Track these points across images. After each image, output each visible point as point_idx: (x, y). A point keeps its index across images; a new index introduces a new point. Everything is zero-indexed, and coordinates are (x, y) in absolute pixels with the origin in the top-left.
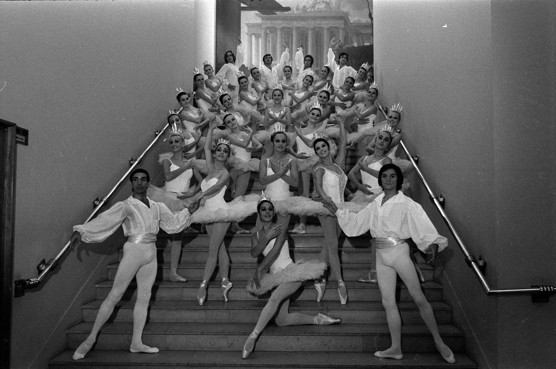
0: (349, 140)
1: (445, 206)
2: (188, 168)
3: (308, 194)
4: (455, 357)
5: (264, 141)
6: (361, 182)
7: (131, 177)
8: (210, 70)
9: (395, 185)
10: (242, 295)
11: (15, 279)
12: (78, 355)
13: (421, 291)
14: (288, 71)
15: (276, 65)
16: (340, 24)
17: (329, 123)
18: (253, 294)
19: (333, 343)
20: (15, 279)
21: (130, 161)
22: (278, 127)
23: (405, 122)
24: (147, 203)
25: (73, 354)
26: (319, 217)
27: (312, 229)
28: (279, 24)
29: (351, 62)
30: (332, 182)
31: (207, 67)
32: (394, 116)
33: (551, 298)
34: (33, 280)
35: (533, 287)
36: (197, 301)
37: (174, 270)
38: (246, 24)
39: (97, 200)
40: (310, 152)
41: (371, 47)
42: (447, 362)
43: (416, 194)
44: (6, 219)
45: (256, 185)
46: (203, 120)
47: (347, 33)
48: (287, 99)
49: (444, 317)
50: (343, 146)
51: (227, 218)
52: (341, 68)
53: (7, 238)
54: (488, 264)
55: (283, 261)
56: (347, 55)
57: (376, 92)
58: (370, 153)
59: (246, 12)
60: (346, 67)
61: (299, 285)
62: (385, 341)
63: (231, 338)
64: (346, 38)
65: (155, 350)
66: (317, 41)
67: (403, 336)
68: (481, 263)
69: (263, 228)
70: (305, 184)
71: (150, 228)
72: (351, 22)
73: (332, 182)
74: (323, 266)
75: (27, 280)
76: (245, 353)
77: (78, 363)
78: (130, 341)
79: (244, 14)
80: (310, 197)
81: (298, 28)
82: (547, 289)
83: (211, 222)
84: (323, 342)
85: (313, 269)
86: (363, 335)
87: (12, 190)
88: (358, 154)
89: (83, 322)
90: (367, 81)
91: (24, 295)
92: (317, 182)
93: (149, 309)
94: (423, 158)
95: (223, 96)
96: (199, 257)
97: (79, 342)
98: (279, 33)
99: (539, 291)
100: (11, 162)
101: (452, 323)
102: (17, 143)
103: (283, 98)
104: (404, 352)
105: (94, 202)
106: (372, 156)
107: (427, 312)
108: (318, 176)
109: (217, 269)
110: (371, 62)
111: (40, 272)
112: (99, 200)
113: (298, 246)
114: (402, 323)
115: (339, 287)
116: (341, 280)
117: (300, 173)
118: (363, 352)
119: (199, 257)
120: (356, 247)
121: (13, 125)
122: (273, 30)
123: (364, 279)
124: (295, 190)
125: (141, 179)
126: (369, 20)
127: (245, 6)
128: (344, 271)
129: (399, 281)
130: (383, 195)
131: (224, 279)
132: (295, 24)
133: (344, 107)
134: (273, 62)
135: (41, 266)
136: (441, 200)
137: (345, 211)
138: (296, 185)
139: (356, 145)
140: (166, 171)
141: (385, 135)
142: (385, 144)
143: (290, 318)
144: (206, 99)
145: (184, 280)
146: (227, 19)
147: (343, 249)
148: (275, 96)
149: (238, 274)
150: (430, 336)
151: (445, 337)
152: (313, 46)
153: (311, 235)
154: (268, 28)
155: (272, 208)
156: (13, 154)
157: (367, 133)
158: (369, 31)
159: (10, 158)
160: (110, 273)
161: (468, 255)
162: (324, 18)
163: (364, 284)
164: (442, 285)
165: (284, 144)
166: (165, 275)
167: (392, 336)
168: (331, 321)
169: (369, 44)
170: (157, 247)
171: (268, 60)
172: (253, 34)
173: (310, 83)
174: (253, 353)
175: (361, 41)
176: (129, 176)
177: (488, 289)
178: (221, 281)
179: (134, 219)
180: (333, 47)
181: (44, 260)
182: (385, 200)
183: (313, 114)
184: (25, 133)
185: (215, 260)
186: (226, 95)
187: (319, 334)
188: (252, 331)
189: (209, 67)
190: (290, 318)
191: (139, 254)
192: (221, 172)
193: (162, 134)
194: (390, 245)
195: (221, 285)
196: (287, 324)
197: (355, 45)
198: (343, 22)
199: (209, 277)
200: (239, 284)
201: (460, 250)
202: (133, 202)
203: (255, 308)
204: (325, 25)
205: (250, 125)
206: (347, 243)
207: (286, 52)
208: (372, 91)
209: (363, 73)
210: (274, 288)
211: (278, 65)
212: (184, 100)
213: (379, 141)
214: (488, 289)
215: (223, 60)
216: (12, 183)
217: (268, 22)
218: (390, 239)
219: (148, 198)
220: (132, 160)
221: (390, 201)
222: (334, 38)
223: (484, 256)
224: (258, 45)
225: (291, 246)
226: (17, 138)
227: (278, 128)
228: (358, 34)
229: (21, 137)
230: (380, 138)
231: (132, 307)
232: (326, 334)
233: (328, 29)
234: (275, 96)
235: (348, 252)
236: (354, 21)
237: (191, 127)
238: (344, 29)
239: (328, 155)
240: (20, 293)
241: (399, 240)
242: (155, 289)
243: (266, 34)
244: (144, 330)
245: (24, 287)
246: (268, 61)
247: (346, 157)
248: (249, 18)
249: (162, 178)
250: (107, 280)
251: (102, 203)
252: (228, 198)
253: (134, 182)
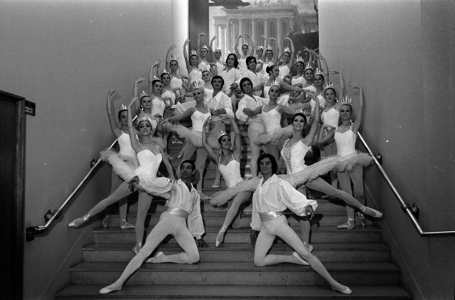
1: (382, 163)
11: (26, 226)
12: (105, 291)
16: (290, 15)
20: (26, 226)
28: (240, 16)
32: (345, 110)
34: (41, 227)
38: (213, 17)
41: (317, 34)
44: (18, 176)
47: (296, 22)
53: (19, 192)
59: (213, 7)
63: (204, 275)
64: (296, 27)
68: (414, 209)
72: (299, 13)
79: (211, 8)
84: (282, 277)
87: (23, 152)
100: (21, 129)
111: (47, 220)
118: (315, 285)
121: (22, 99)
122: (236, 21)
126: (315, 11)
127: (212, 2)
132: (254, 16)
135: (48, 215)
146: (198, 13)
158: (315, 20)
159: (20, 126)
161: (403, 203)
162: (277, 11)
169: (314, 31)
175: (308, 30)
177: (421, 232)
179: (175, 194)
181: (50, 210)
184: (32, 105)
197: (303, 32)
198: (292, 13)
201: (393, 194)
204: (278, 16)
214: (421, 232)
223: (416, 203)
226: (26, 109)
228: (306, 24)
233: (281, 20)
238: (293, 19)
243: (230, 25)
245: (33, 233)
248: (216, 12)
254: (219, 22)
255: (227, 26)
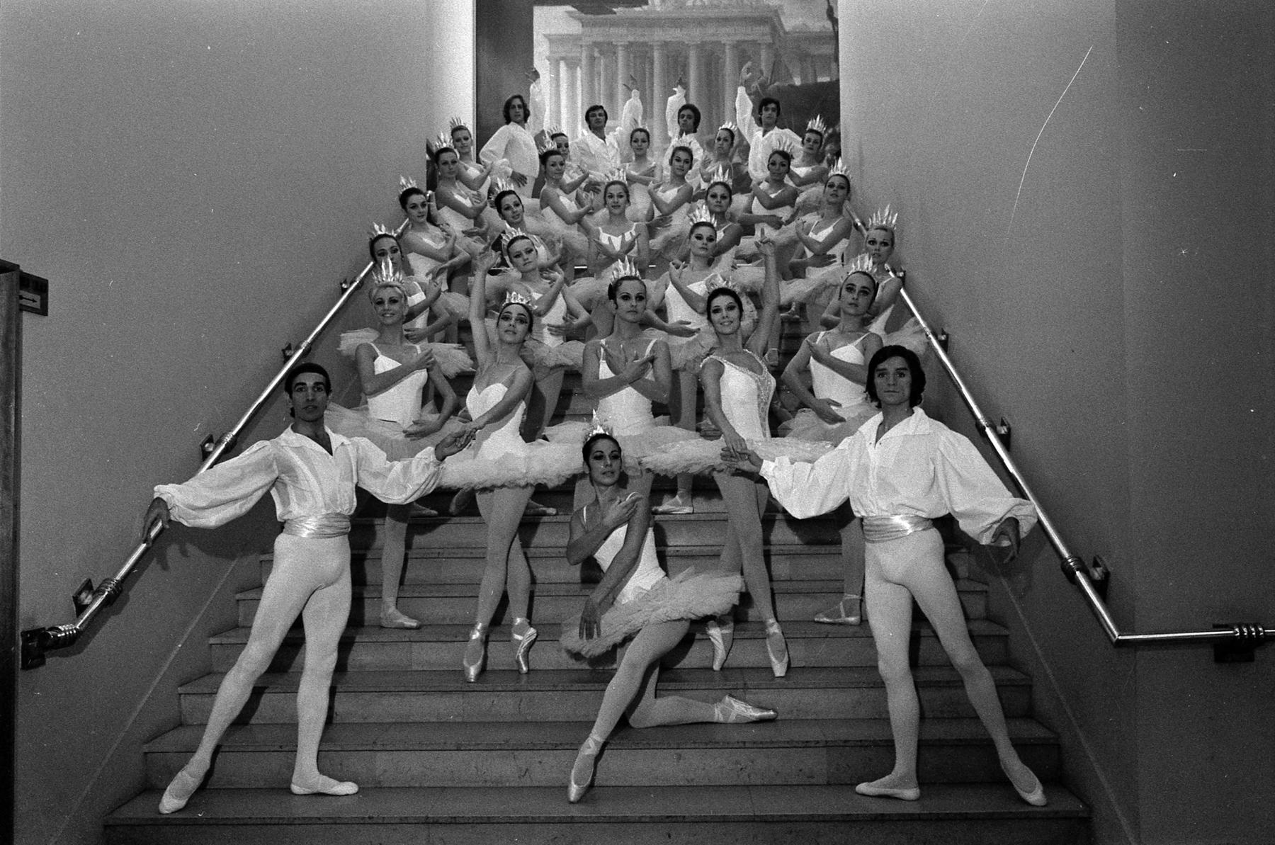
0: (784, 300)
2: (419, 367)
3: (693, 424)
4: (1044, 792)
5: (590, 301)
6: (811, 390)
7: (289, 383)
8: (466, 139)
9: (907, 392)
10: (550, 657)
12: (170, 802)
13: (969, 642)
14: (639, 141)
15: (613, 129)
16: (759, 33)
17: (739, 257)
18: (577, 656)
19: (763, 765)
21: (284, 351)
22: (623, 269)
23: (908, 252)
24: (326, 443)
25: (160, 801)
26: (715, 474)
27: (702, 505)
28: (621, 36)
29: (790, 122)
30: (740, 391)
31: (457, 130)
32: (879, 240)
33: (1259, 654)
34: (66, 629)
35: (1216, 627)
36: (463, 673)
37: (389, 599)
39: (210, 440)
40: (697, 321)
41: (834, 86)
42: (1028, 804)
43: (948, 413)
45: (577, 404)
46: (452, 256)
47: (777, 55)
48: (640, 202)
49: (1018, 700)
50: (768, 309)
51: (525, 475)
52: (765, 133)
54: (1112, 577)
55: (646, 575)
56: (777, 103)
57: (846, 184)
58: (828, 325)
60: (776, 130)
61: (682, 628)
62: (878, 756)
63: (524, 758)
64: (776, 67)
65: (349, 788)
66: (709, 73)
67: (922, 745)
68: (1097, 573)
69: (597, 500)
70: (682, 400)
71: (334, 501)
73: (740, 391)
74: (733, 584)
75: (51, 629)
76: (574, 791)
77: (170, 822)
78: (291, 768)
80: (698, 430)
81: (665, 44)
82: (1250, 632)
83: (488, 484)
85: (711, 592)
86: (827, 745)
88: (804, 329)
89: (180, 724)
90: (825, 165)
91: (43, 663)
92: (710, 393)
93: (333, 692)
94: (957, 337)
95: (504, 194)
96: (456, 570)
97: (171, 774)
98: (621, 54)
99: (1232, 637)
101: (1030, 714)
102: (21, 310)
103: (628, 201)
104: (921, 783)
105: (202, 446)
106: (834, 331)
107: (981, 689)
108: (708, 380)
109: (504, 601)
110: (832, 118)
111: (81, 608)
112: (215, 440)
113: (676, 541)
114: (922, 717)
115: (769, 635)
116: (772, 621)
117: (675, 373)
118: (829, 784)
119: (456, 570)
120: (807, 543)
122: (607, 49)
123: (827, 616)
124: (664, 409)
125: (313, 388)
126: (828, 25)
128: (777, 597)
129: (918, 617)
130: (879, 417)
131: (518, 620)
132: (659, 35)
133: (777, 224)
134: (609, 123)
135: (83, 595)
136: (1003, 430)
137: (781, 464)
138: (664, 397)
139: (802, 307)
140: (365, 372)
141: (860, 282)
142: (863, 301)
143: (661, 708)
144: (458, 208)
145: (414, 624)
147: (772, 548)
148: (611, 196)
149: (544, 610)
150: (989, 746)
151: (1023, 748)
152: (699, 79)
153: (703, 517)
154: (596, 44)
155: (617, 454)
156: (13, 337)
157: (831, 281)
158: (827, 50)
160: (241, 609)
161: (1066, 555)
162: (725, 21)
163: (829, 627)
164: (1006, 627)
165: (640, 305)
166: (369, 613)
167: (897, 746)
168: (757, 714)
169: (826, 79)
170: (352, 548)
171: (596, 119)
172: (563, 58)
173: (686, 166)
174: (590, 792)
176: (283, 385)
178: (511, 625)
179: (295, 479)
180: (747, 84)
182: (882, 429)
183: (699, 237)
184: (40, 286)
185: (501, 576)
186: (511, 192)
187: (727, 745)
188: (587, 737)
189: (464, 133)
190: (661, 708)
191: (306, 560)
192: (513, 368)
193: (357, 288)
194: (896, 533)
195: (510, 634)
196: (654, 724)
198: (767, 29)
199: (490, 617)
200: (548, 631)
202: (292, 442)
203: (576, 686)
204: (727, 36)
205: (562, 263)
206: (781, 534)
207: (635, 100)
208: (837, 181)
209: (815, 142)
210: (628, 639)
211: (619, 128)
212: (415, 206)
213: (849, 297)
215: (501, 117)
216: (13, 404)
217: (596, 30)
218: (897, 520)
219: (328, 431)
220: (289, 348)
221: (896, 432)
222: (749, 64)
224: (572, 85)
225: (660, 542)
226: (21, 298)
227: (625, 268)
228: (803, 57)
229: (31, 298)
230: (850, 288)
231: (294, 689)
232: (743, 745)
234: (611, 196)
235: (791, 555)
236: (794, 28)
237: (422, 267)
238: (770, 46)
239: (735, 332)
240: (34, 659)
241: (918, 521)
242: (345, 645)
243: (592, 60)
244: (321, 740)
245: (43, 644)
246: (598, 121)
247: (781, 338)
248: (550, 23)
249: (355, 386)
250: (236, 626)
251: (223, 447)
252: (530, 432)
253: (295, 395)
254: (562, 51)
255: (584, 62)
